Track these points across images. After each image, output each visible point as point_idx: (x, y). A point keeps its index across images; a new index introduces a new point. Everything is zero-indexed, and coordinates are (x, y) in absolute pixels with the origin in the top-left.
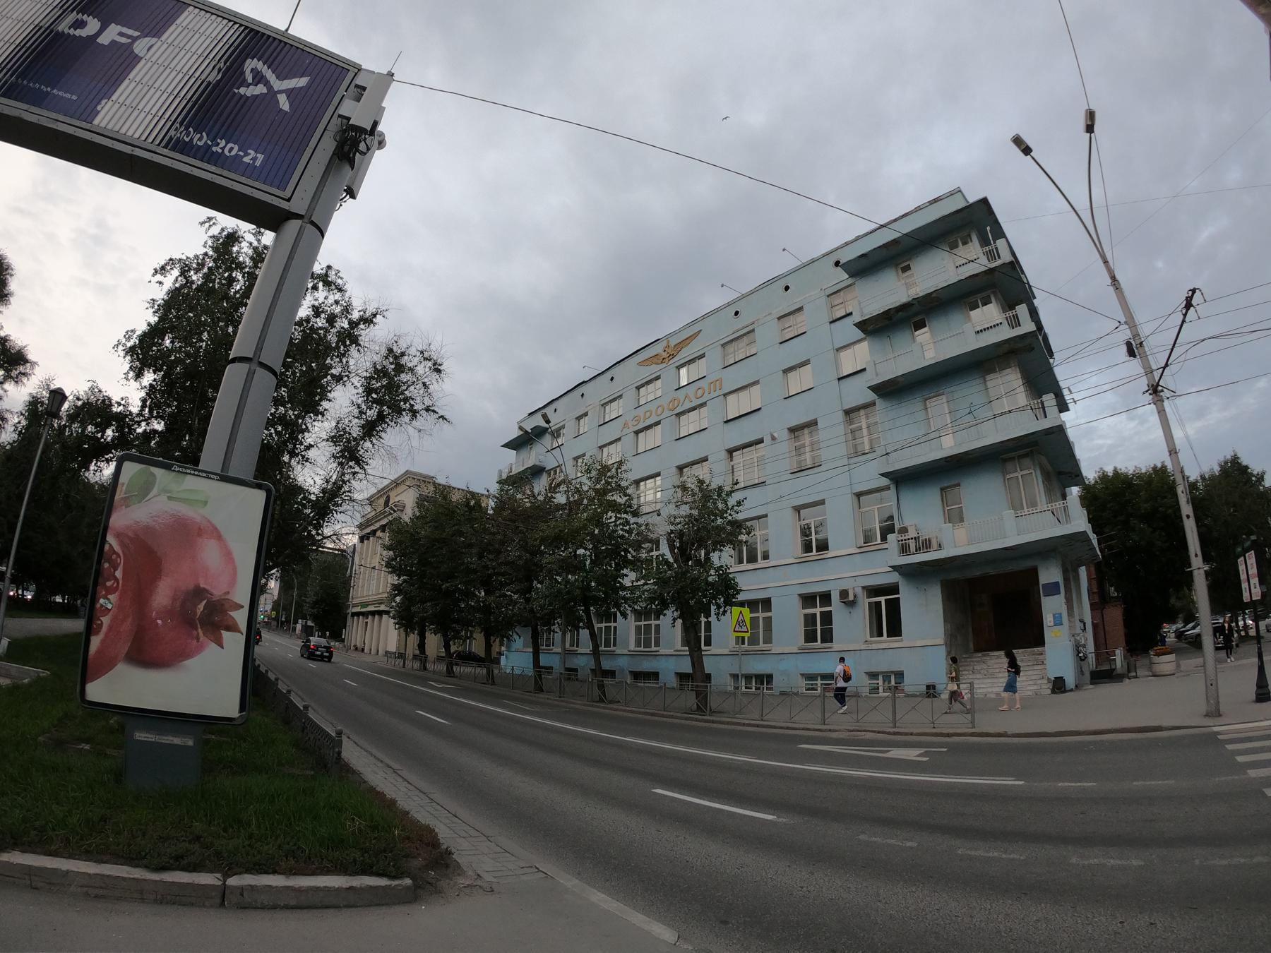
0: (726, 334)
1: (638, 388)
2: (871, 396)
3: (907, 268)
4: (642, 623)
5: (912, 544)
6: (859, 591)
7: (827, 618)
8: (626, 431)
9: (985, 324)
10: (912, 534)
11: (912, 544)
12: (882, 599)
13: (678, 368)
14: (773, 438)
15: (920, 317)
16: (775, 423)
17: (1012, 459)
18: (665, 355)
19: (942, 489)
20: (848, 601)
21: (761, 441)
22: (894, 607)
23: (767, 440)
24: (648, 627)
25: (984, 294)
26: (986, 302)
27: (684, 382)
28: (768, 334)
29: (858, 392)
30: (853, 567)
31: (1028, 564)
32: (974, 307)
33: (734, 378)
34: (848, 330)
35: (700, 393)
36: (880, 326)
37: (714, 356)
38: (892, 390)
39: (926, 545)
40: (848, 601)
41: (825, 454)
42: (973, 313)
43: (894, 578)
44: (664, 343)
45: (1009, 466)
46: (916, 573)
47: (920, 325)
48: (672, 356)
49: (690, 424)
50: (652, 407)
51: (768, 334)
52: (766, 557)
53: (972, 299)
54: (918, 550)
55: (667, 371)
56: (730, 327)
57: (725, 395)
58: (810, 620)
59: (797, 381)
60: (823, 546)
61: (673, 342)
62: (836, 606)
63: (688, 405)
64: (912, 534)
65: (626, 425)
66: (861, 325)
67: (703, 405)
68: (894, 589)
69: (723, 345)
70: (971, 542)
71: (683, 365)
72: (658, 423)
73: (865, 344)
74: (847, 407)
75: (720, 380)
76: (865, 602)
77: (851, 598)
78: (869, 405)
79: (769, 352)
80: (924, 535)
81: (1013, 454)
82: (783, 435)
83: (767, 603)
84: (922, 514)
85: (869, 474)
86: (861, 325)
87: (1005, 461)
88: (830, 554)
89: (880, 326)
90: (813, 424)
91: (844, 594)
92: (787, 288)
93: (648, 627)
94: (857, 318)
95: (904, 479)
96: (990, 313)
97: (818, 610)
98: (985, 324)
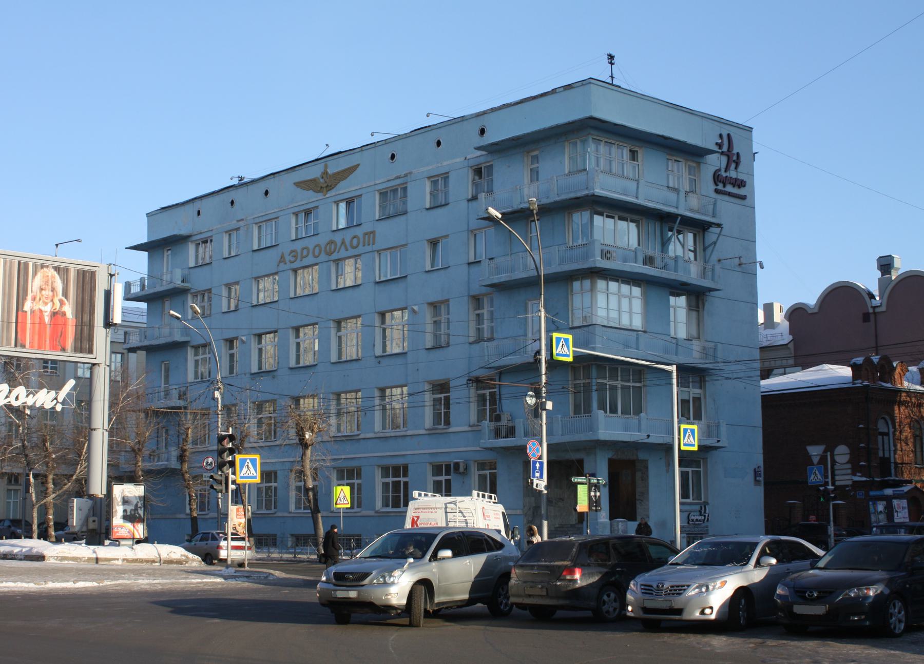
3: (535, 159)
13: (337, 203)
43: (488, 457)
48: (329, 188)
51: (420, 194)
56: (384, 175)
57: (379, 252)
65: (282, 259)
77: (461, 469)
88: (451, 430)
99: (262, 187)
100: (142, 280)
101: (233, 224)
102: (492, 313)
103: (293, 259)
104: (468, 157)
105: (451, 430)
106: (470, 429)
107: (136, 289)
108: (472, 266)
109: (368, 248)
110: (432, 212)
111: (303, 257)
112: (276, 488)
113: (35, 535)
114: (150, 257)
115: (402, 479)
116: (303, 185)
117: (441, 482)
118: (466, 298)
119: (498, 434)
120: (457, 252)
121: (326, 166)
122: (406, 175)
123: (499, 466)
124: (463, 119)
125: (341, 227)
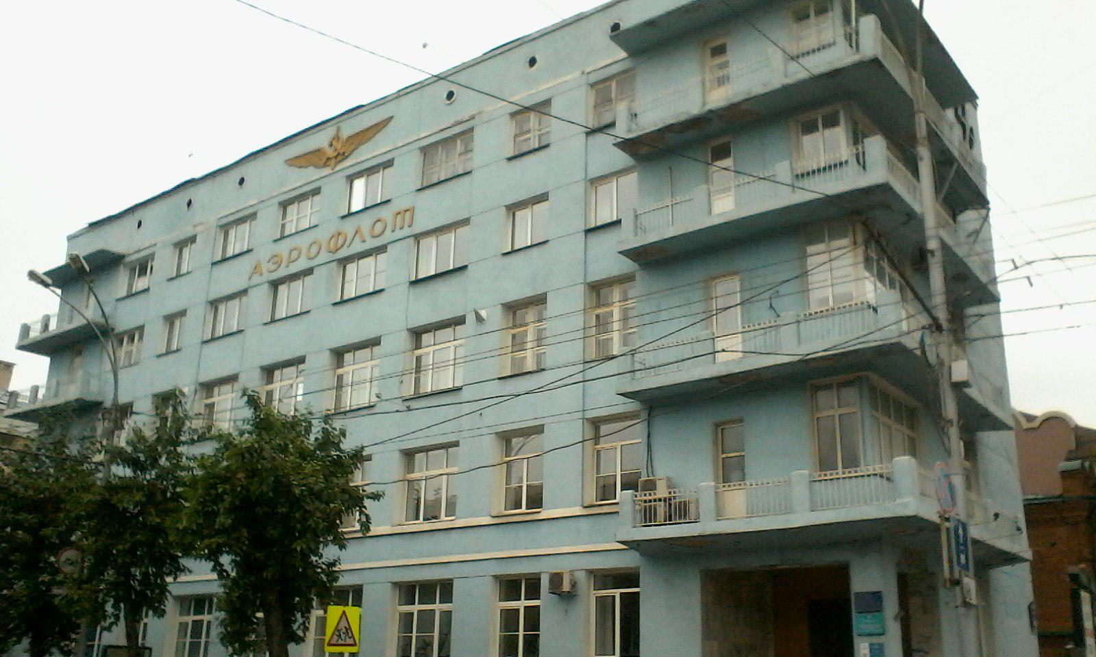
0: (428, 131)
1: (284, 205)
2: (627, 265)
3: (720, 51)
4: (416, 608)
5: (661, 510)
6: (581, 576)
7: (533, 617)
8: (256, 279)
9: (836, 161)
10: (662, 492)
11: (661, 510)
12: (617, 593)
13: (351, 179)
14: (479, 319)
15: (721, 141)
16: (484, 294)
17: (828, 387)
18: (330, 152)
19: (717, 425)
20: (566, 595)
21: (460, 321)
22: (631, 606)
23: (471, 319)
24: (426, 617)
25: (828, 110)
26: (831, 122)
27: (357, 205)
28: (494, 139)
29: (607, 258)
30: (577, 539)
31: (830, 558)
32: (810, 128)
33: (434, 208)
34: (606, 155)
35: (379, 227)
36: (659, 150)
37: (408, 170)
38: (659, 259)
39: (679, 511)
40: (566, 595)
41: (552, 355)
42: (807, 140)
43: (630, 560)
44: (330, 132)
45: (822, 397)
46: (666, 554)
47: (721, 152)
48: (341, 156)
49: (361, 277)
50: (302, 242)
51: (494, 139)
52: (451, 510)
53: (809, 116)
54: (669, 519)
55: (333, 187)
56: (435, 120)
57: (418, 237)
58: (509, 618)
59: (527, 228)
60: (536, 500)
61: (349, 129)
62: (545, 602)
63: (358, 247)
64: (662, 492)
65: (256, 269)
66: (628, 145)
67: (382, 249)
68: (627, 578)
69: (425, 150)
70: (751, 514)
71: (359, 175)
72: (309, 272)
73: (633, 177)
74: (592, 278)
75: (410, 210)
76: (590, 596)
77: (566, 587)
78: (625, 279)
79: (492, 176)
80: (682, 495)
81: (827, 380)
82: (494, 316)
83: (445, 589)
84: (684, 465)
85: (606, 397)
86: (628, 145)
87: (817, 389)
88: (545, 514)
89: (659, 150)
90: (539, 300)
91: (556, 579)
92: (532, 62)
93: (426, 617)
94: (623, 131)
95: (662, 405)
96: (830, 144)
97: (521, 604)
98: (836, 161)
99: (235, 175)
100: (35, 389)
101: (187, 232)
102: (625, 311)
103: (273, 267)
104: (588, 69)
105: (545, 514)
106: (585, 512)
107: (35, 334)
108: (590, 236)
109: (399, 234)
110: (516, 163)
111: (290, 262)
112: (209, 623)
113: (411, 634)
114: (63, 300)
115: (438, 607)
116: (299, 162)
117: (517, 611)
118: (581, 288)
119: (648, 516)
120: (555, 222)
121: (338, 129)
122: (473, 118)
123: (643, 579)
124: (580, 18)
125: (353, 210)
